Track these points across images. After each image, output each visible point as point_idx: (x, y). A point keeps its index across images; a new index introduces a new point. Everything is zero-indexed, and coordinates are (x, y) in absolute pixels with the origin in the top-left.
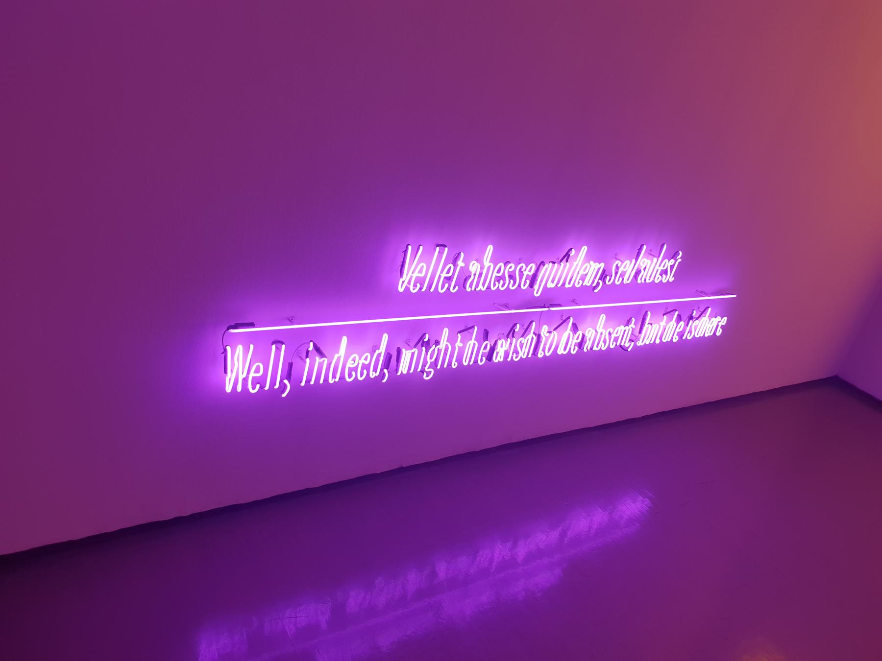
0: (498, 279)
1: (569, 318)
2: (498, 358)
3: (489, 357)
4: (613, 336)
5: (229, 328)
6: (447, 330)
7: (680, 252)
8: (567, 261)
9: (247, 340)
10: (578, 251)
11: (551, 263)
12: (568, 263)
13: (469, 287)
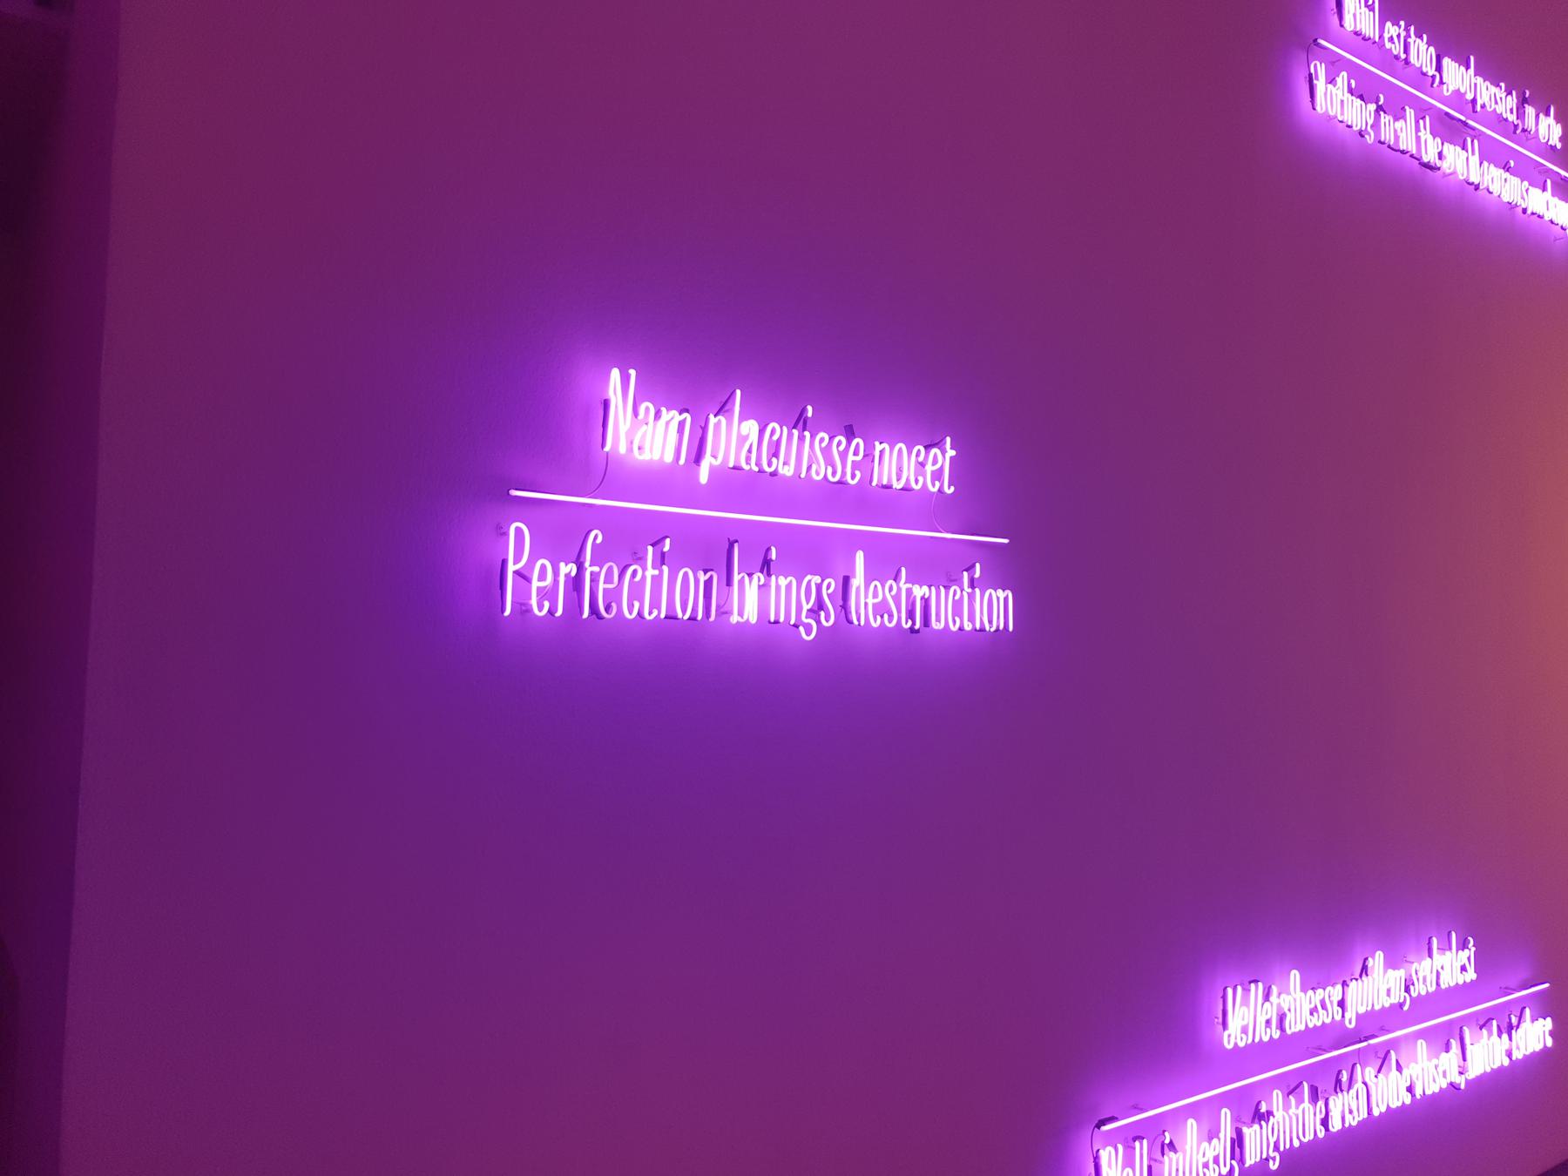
0: (1313, 1011)
1: (1388, 1052)
2: (1336, 1125)
3: (1325, 1122)
4: (1441, 1070)
5: (1098, 1126)
6: (1424, 1043)
7: (1469, 938)
8: (1367, 975)
9: (1111, 1139)
10: (1373, 958)
11: (1354, 981)
12: (1369, 977)
13: (1277, 1028)
